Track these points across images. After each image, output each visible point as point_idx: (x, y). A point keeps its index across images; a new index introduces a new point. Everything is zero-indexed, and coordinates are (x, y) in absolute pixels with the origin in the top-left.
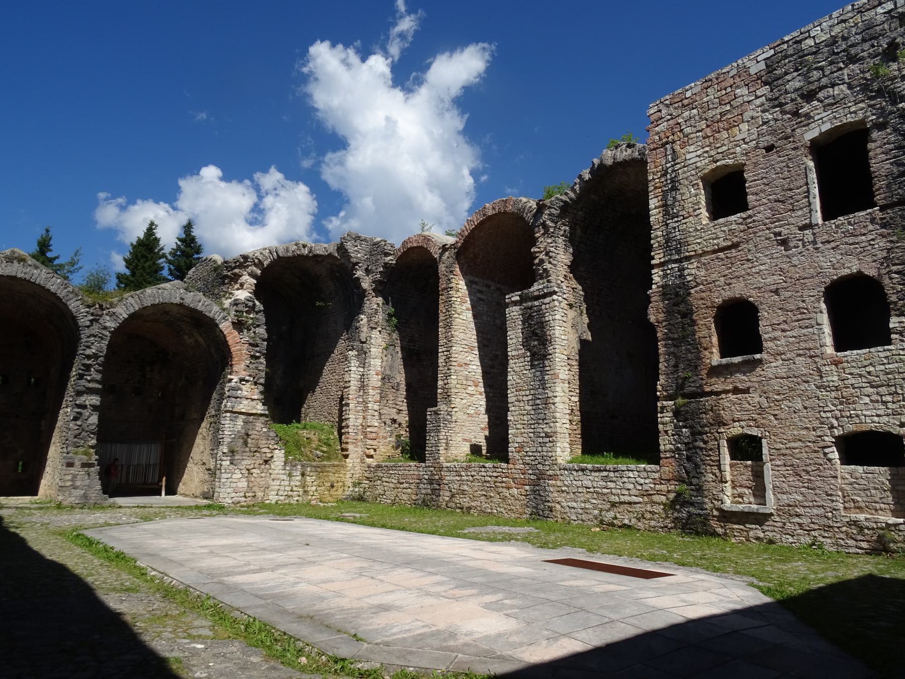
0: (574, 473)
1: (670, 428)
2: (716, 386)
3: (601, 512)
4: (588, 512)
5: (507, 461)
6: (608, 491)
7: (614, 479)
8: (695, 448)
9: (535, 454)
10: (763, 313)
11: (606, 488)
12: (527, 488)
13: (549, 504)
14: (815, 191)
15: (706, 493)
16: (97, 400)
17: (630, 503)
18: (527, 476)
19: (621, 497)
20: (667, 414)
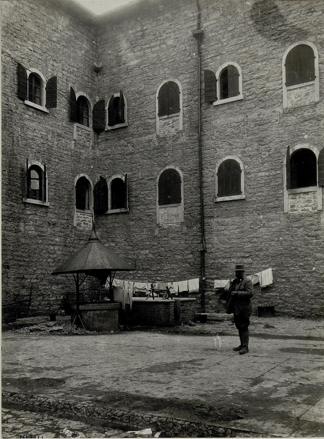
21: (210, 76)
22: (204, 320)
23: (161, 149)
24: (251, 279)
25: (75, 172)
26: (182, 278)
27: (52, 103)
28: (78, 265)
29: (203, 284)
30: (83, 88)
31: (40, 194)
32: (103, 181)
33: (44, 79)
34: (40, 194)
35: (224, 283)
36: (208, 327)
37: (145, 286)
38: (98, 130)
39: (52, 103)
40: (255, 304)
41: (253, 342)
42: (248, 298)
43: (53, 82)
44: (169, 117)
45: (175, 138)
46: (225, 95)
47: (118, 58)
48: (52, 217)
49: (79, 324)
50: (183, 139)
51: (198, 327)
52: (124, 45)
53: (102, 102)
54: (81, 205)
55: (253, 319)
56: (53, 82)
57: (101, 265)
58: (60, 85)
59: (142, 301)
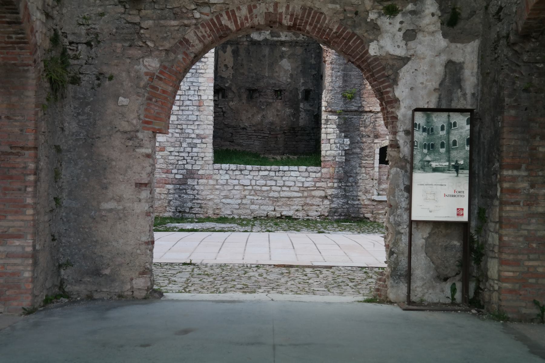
0: (231, 172)
1: (332, 137)
2: (375, 108)
3: (290, 209)
4: (246, 206)
5: (214, 163)
6: (269, 188)
7: (275, 178)
8: (353, 153)
9: (182, 154)
10: (451, 59)
11: (265, 185)
12: (171, 187)
13: (199, 201)
14: (306, 14)
15: (114, 163)
16: (189, 182)
17: (289, 198)
18: (171, 176)
19: (281, 193)
20: (331, 126)
21: (451, 123)
22: (449, 170)
23: (441, 138)
24: (459, 163)
25: (424, 142)
26: (445, 162)
27: (419, 129)
28: (424, 160)
29: (449, 164)
30: (425, 125)
31: (417, 146)
32: (429, 144)
33: (418, 124)
34: (417, 146)
35: (453, 163)
36: (450, 172)
37: (437, 164)
38: (428, 134)
39: (419, 129)
40: (460, 167)
41: (459, 175)
42: (458, 166)
43: (419, 124)
44: (290, 169)
45: (444, 135)
46: (454, 127)
47: (432, 120)
48: (419, 150)
49: (424, 171)
50: (445, 136)
51: (448, 172)
52: (434, 117)
53: (429, 128)
54: (425, 148)
55: (459, 170)
56: (419, 124)
57: (521, 239)
58: (421, 125)
59: (324, 69)
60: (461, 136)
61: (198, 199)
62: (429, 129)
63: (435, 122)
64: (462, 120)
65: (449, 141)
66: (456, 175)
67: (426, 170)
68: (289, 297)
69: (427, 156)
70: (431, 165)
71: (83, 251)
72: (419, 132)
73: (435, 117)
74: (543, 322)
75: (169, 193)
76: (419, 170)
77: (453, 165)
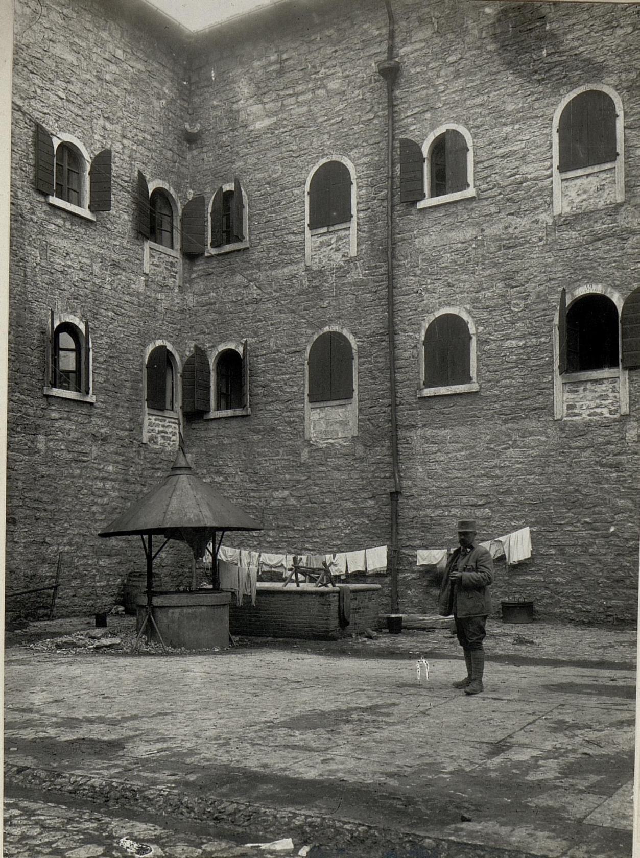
21: (411, 149)
22: (395, 627)
23: (314, 293)
27: (100, 203)
29: (394, 558)
30: (160, 174)
32: (200, 354)
33: (87, 155)
35: (434, 557)
36: (404, 642)
37: (282, 560)
38: (191, 256)
39: (100, 203)
40: (495, 597)
41: (491, 673)
43: (103, 160)
45: (342, 272)
46: (438, 190)
47: (232, 115)
48: (98, 425)
49: (150, 631)
50: (357, 274)
51: (384, 641)
52: (244, 88)
53: (200, 201)
54: (157, 401)
55: (492, 627)
56: (103, 160)
60: (509, 279)
61: (275, 614)
62: (195, 207)
63: (254, 139)
64: (522, 117)
65: (391, 330)
66: (459, 670)
67: (163, 619)
68: (84, 346)
69: (184, 480)
70: (215, 571)
71: (614, 475)
72: (93, 243)
73: (259, 95)
74: (5, 855)
75: (600, 606)
76: (101, 622)
77: (433, 576)
